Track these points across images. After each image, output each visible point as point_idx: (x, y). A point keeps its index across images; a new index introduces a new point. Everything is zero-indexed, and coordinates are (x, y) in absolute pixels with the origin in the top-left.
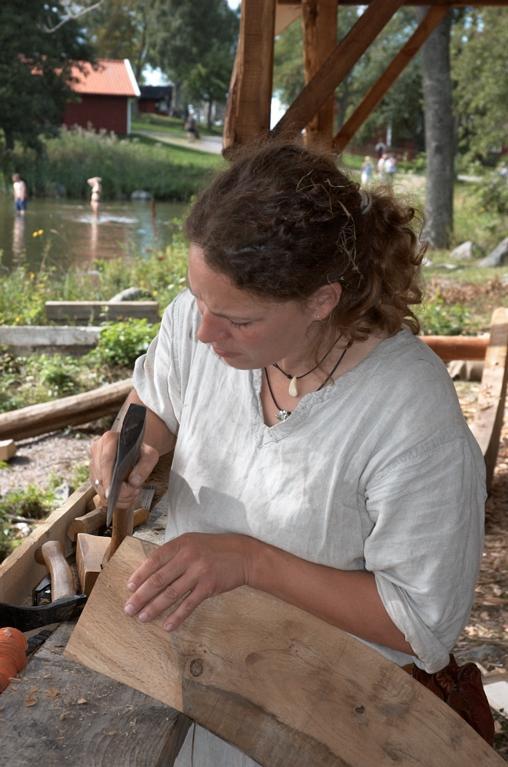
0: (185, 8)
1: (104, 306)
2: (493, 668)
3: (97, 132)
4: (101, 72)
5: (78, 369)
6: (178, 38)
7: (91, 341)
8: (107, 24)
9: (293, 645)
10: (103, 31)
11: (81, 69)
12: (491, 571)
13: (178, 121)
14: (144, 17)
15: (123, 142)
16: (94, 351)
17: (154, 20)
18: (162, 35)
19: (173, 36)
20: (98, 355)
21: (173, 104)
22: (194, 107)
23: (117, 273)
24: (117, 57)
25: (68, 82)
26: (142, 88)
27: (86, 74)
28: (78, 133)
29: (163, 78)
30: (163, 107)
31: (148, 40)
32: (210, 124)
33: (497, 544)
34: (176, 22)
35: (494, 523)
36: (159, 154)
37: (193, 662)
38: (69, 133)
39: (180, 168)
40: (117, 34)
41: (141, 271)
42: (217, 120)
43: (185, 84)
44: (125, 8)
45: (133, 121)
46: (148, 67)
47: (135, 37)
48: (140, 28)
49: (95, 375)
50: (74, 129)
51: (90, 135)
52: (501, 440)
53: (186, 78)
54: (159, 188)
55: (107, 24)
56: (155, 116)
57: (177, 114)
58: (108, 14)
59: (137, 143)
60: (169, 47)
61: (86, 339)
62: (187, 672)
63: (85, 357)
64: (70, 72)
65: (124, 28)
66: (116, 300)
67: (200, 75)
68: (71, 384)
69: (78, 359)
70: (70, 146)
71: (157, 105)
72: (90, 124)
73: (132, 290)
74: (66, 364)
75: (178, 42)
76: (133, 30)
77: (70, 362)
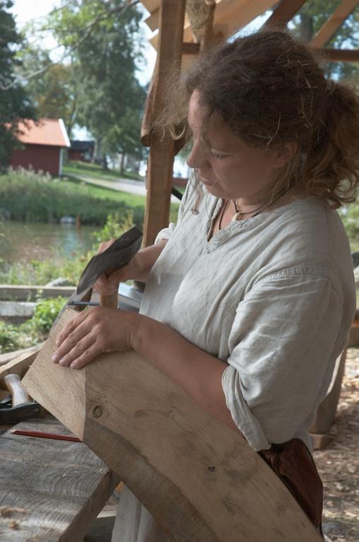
0: (108, 83)
1: (39, 289)
2: (336, 538)
3: (36, 172)
4: (41, 127)
5: (17, 334)
6: (100, 105)
7: (28, 313)
8: (47, 93)
9: (172, 411)
10: (43, 98)
11: (26, 125)
12: (334, 474)
13: (98, 167)
14: (75, 89)
15: (56, 181)
16: (31, 320)
17: (82, 91)
18: (89, 102)
19: (97, 104)
20: (34, 323)
21: (95, 154)
22: (111, 157)
23: (49, 271)
24: (53, 116)
25: (15, 134)
26: (72, 142)
27: (29, 128)
28: (21, 172)
29: (87, 135)
30: (87, 157)
31: (78, 106)
32: (123, 170)
33: (340, 456)
34: (99, 94)
35: (337, 442)
36: (83, 190)
37: (97, 407)
38: (14, 173)
39: (99, 201)
40: (55, 101)
41: (68, 270)
42: (128, 167)
43: (105, 139)
44: (61, 83)
45: (64, 165)
46: (77, 126)
47: (68, 104)
48: (72, 97)
49: (30, 339)
50: (19, 169)
51: (30, 174)
52: (343, 386)
53: (105, 135)
54: (82, 215)
55: (47, 93)
56: (81, 163)
57: (97, 162)
58: (48, 86)
59: (67, 181)
60: (93, 112)
61: (25, 311)
62: (91, 413)
63: (23, 325)
64: (17, 126)
65: (60, 96)
66: (49, 286)
67: (116, 133)
68: (12, 345)
69: (18, 327)
70: (15, 182)
71: (82, 155)
72: (30, 166)
73: (60, 280)
74: (9, 330)
75: (100, 108)
76: (66, 99)
77: (12, 329)
